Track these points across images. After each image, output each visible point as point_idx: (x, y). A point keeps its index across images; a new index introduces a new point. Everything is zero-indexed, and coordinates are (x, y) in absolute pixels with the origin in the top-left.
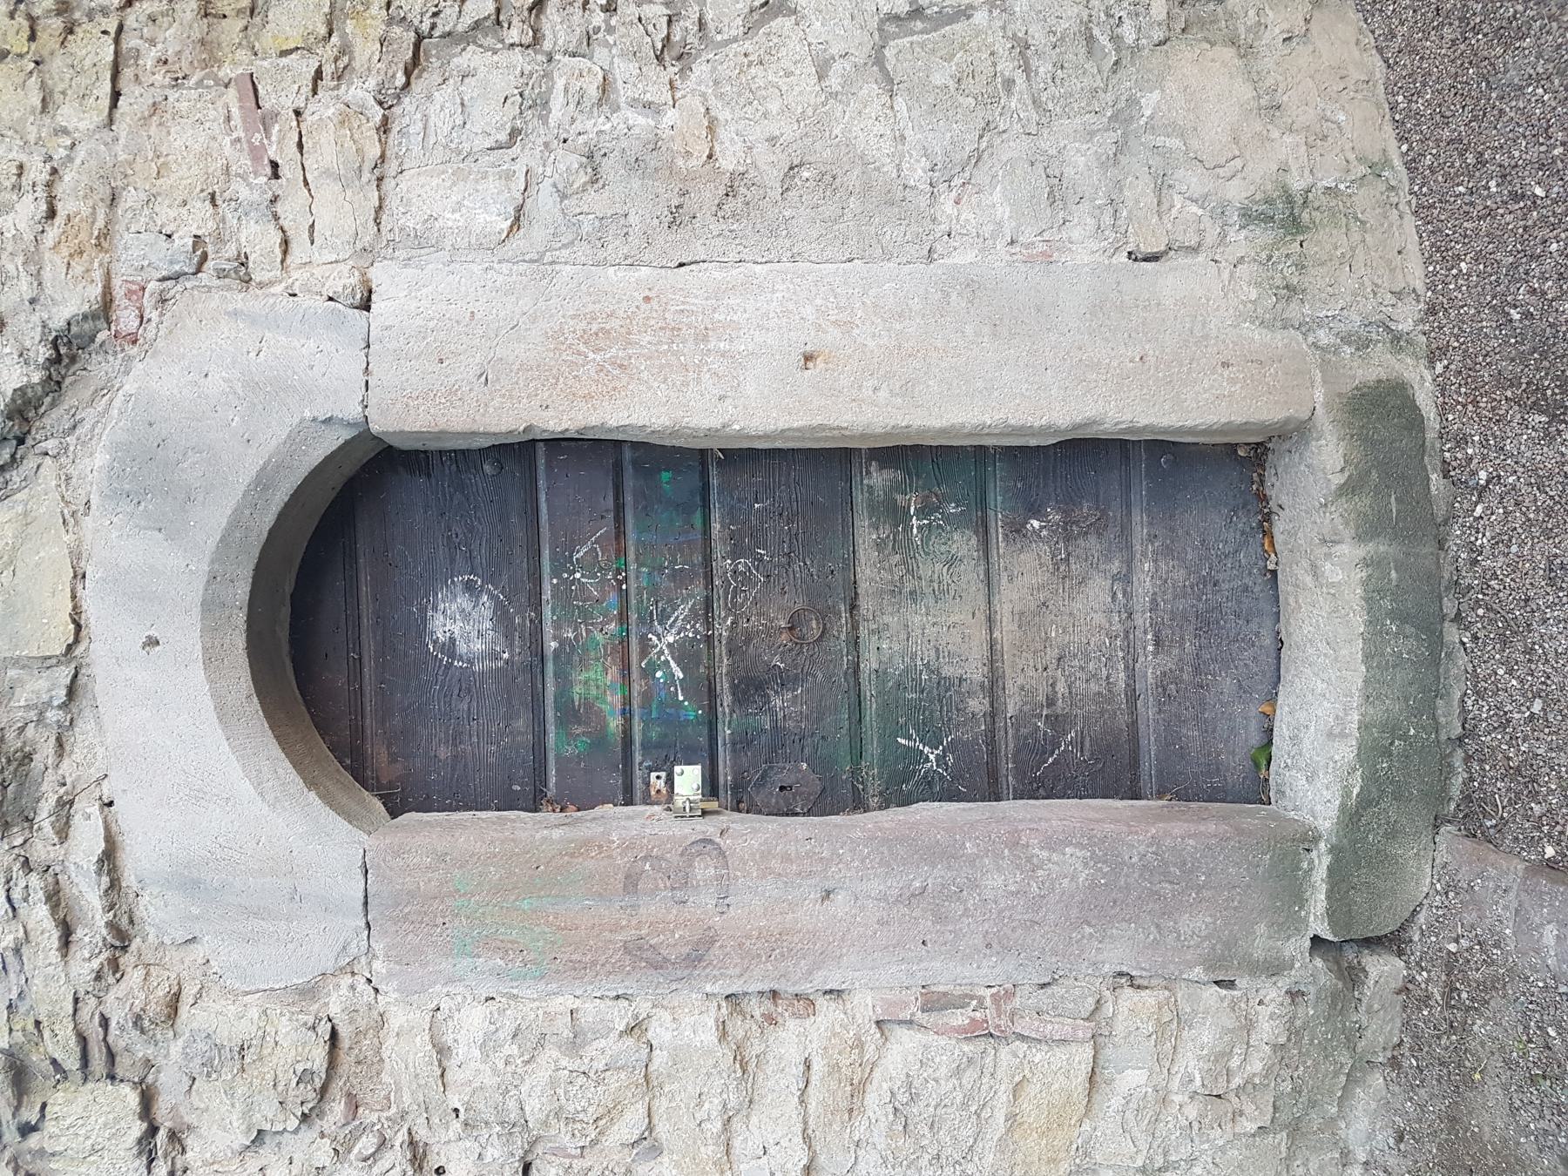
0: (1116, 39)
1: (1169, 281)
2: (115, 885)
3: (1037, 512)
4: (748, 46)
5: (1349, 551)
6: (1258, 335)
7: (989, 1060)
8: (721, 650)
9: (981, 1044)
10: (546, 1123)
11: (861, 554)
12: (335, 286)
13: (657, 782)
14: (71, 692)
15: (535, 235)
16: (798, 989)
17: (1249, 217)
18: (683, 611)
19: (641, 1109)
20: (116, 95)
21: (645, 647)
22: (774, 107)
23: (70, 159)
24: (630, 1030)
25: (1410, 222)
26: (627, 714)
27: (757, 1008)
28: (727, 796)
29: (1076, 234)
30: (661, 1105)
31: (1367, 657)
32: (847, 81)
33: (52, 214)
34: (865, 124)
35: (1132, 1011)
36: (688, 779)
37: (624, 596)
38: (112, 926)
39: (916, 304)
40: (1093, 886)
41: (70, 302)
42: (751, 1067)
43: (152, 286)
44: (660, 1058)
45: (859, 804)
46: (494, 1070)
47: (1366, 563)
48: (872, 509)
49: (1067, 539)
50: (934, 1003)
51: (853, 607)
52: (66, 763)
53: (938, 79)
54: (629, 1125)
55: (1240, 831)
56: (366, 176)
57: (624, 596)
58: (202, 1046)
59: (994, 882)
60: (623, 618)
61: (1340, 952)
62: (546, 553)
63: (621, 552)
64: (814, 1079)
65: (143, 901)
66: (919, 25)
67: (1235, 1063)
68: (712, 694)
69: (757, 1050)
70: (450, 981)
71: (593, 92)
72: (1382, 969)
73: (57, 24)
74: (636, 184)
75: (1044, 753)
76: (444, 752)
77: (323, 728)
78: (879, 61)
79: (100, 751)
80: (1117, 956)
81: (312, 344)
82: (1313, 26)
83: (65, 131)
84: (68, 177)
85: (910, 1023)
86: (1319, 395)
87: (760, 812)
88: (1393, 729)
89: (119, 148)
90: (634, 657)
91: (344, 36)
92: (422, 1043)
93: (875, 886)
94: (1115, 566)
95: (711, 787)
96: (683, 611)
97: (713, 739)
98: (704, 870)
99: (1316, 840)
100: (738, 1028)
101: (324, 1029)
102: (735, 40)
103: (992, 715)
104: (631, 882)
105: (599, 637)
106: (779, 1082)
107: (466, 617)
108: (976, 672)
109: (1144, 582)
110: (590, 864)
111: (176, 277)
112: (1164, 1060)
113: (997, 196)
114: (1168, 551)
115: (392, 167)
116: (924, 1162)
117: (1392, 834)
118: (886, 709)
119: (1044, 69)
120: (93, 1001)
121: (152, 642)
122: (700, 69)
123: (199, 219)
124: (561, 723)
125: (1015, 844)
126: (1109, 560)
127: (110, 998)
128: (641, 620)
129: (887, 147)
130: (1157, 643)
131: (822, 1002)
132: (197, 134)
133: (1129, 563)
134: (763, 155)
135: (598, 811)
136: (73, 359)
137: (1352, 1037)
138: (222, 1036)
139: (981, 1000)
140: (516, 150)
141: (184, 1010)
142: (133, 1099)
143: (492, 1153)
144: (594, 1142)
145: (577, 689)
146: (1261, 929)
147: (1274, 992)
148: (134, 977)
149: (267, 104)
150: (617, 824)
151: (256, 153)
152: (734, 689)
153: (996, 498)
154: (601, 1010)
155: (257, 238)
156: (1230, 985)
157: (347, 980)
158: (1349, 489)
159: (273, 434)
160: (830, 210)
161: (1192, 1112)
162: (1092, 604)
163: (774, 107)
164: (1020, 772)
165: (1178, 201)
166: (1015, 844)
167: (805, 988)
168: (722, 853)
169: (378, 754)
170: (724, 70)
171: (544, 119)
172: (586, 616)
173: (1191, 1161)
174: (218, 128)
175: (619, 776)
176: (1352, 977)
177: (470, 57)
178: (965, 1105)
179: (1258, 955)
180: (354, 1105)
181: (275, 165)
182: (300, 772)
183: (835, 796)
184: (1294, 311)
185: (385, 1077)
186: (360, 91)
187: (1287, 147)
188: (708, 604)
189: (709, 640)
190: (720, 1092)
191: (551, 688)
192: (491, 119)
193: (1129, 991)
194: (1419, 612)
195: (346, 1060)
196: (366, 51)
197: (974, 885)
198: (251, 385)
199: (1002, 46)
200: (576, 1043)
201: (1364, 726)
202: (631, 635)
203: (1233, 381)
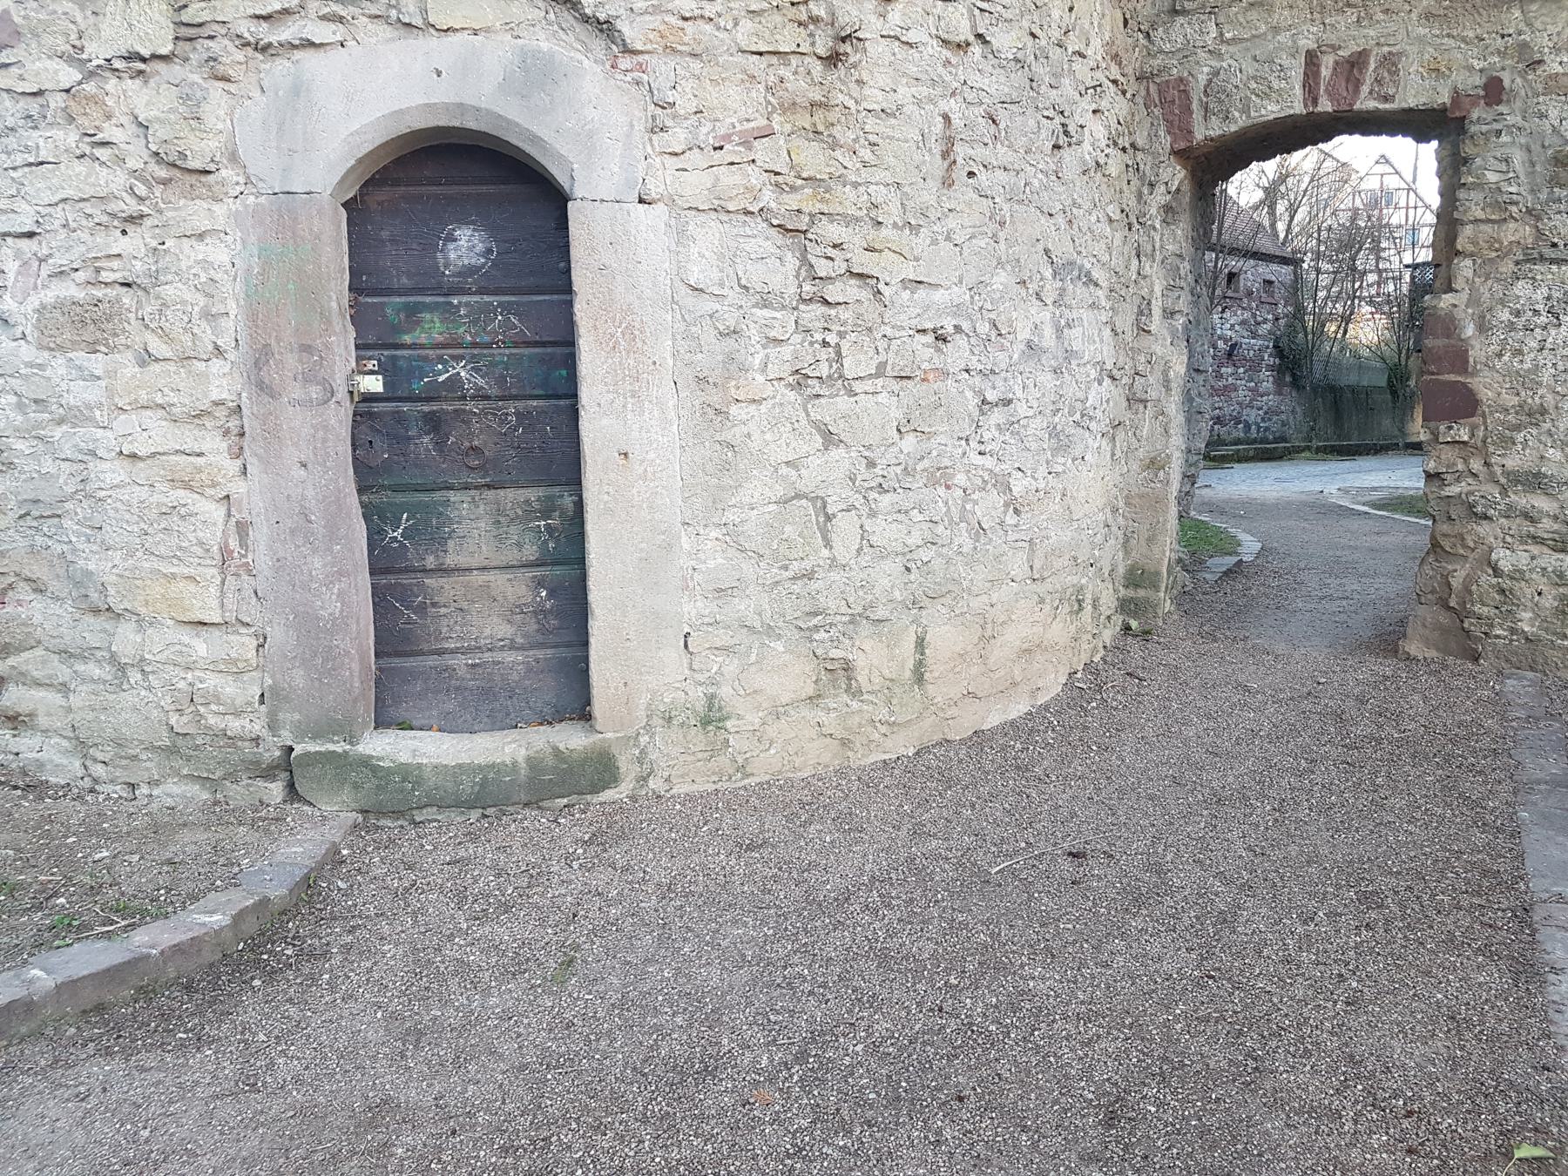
0: (816, 628)
1: (672, 655)
2: (295, 47)
3: (551, 595)
4: (804, 422)
5: (522, 754)
6: (643, 701)
7: (209, 562)
8: (457, 405)
9: (218, 557)
10: (158, 297)
11: (521, 491)
12: (650, 181)
13: (372, 365)
14: (409, 25)
15: (688, 299)
16: (246, 447)
17: (711, 698)
18: (481, 382)
19: (169, 355)
20: (761, 54)
21: (458, 358)
22: (768, 437)
23: (719, 28)
24: (217, 348)
25: (711, 787)
26: (410, 347)
27: (233, 424)
28: (364, 407)
29: (699, 604)
30: (171, 367)
31: (460, 766)
32: (785, 478)
33: (685, 19)
34: (760, 489)
35: (243, 645)
36: (374, 384)
37: (488, 346)
38: (270, 45)
39: (658, 516)
40: (318, 619)
41: (630, 31)
42: (197, 421)
43: (645, 77)
44: (201, 366)
45: (361, 491)
46: (190, 267)
47: (515, 763)
48: (550, 498)
49: (534, 612)
50: (242, 529)
51: (489, 486)
52: (365, 19)
53: (788, 529)
54: (157, 347)
55: (355, 701)
56: (716, 202)
57: (488, 346)
58: (199, 94)
59: (317, 563)
60: (474, 345)
61: (286, 766)
62: (513, 298)
63: (516, 345)
64: (191, 459)
65: (288, 64)
66: (822, 519)
67: (213, 707)
68: (429, 400)
69: (208, 424)
70: (243, 241)
71: (772, 334)
72: (275, 790)
73: (804, 17)
74: (720, 358)
75: (402, 601)
76: (385, 234)
77: (398, 161)
78: (797, 496)
79: (374, 40)
80: (276, 634)
81: (616, 169)
82: (829, 740)
83: (736, 24)
84: (708, 28)
85: (229, 515)
86: (610, 735)
87: (353, 428)
88: (418, 783)
89: (726, 57)
90: (450, 351)
91: (802, 187)
92: (205, 225)
93: (310, 493)
94: (520, 640)
95: (369, 398)
96: (481, 382)
97: (400, 399)
98: (315, 392)
99: (351, 743)
100: (221, 412)
101: (212, 167)
102: (808, 415)
103: (424, 571)
104: (306, 349)
105: (462, 330)
106: (188, 438)
107: (471, 249)
108: (450, 560)
109: (510, 657)
110: (316, 325)
111: (651, 91)
112: (214, 666)
113: (720, 561)
114: (529, 670)
115: (724, 217)
116: (142, 525)
117: (356, 786)
118: (426, 508)
119: (797, 587)
120: (223, 32)
121: (439, 74)
122: (792, 395)
123: (685, 105)
124: (406, 305)
125: (340, 573)
126: (523, 636)
127: (226, 42)
128: (474, 356)
129: (747, 500)
130: (473, 666)
131: (239, 462)
132: (738, 104)
133: (522, 648)
134: (739, 431)
135: (351, 328)
136: (601, 31)
137: (231, 776)
138: (205, 107)
139: (245, 556)
140: (737, 289)
141: (221, 84)
142: (164, 51)
143: (138, 264)
144: (147, 327)
145: (428, 316)
146: (297, 716)
147: (258, 727)
148: (239, 56)
149: (756, 143)
150: (342, 342)
151: (728, 137)
152: (433, 413)
153: (558, 571)
154: (230, 329)
155: (677, 137)
156: (262, 702)
157: (242, 180)
158: (557, 752)
159: (563, 146)
160: (710, 468)
161: (182, 685)
162: (498, 628)
163: (768, 437)
164: (389, 587)
165: (720, 659)
166: (340, 573)
167: (247, 452)
168: (326, 402)
169: (382, 195)
170: (788, 409)
171: (756, 305)
172: (475, 322)
173: (149, 689)
174: (742, 114)
175: (374, 340)
176: (268, 773)
177: (792, 261)
178: (180, 548)
179: (281, 716)
180: (165, 182)
181: (721, 148)
182: (367, 155)
183: (367, 476)
184: (657, 721)
185: (182, 202)
186: (768, 197)
187: (754, 719)
188: (487, 398)
189: (464, 398)
190: (182, 402)
191: (428, 299)
192: (755, 275)
193: (255, 643)
194: (487, 796)
195: (193, 179)
196: (792, 201)
197: (315, 551)
198: (590, 132)
199: (808, 564)
200: (208, 315)
201: (420, 766)
202: (461, 353)
203: (616, 689)
